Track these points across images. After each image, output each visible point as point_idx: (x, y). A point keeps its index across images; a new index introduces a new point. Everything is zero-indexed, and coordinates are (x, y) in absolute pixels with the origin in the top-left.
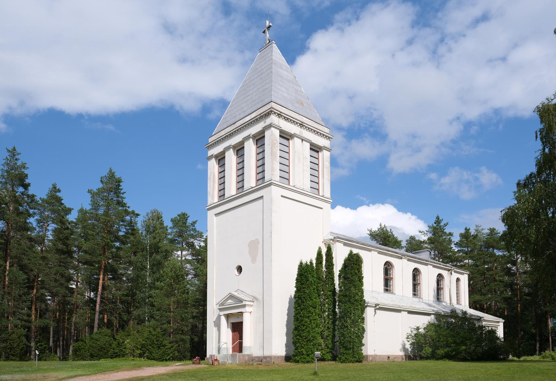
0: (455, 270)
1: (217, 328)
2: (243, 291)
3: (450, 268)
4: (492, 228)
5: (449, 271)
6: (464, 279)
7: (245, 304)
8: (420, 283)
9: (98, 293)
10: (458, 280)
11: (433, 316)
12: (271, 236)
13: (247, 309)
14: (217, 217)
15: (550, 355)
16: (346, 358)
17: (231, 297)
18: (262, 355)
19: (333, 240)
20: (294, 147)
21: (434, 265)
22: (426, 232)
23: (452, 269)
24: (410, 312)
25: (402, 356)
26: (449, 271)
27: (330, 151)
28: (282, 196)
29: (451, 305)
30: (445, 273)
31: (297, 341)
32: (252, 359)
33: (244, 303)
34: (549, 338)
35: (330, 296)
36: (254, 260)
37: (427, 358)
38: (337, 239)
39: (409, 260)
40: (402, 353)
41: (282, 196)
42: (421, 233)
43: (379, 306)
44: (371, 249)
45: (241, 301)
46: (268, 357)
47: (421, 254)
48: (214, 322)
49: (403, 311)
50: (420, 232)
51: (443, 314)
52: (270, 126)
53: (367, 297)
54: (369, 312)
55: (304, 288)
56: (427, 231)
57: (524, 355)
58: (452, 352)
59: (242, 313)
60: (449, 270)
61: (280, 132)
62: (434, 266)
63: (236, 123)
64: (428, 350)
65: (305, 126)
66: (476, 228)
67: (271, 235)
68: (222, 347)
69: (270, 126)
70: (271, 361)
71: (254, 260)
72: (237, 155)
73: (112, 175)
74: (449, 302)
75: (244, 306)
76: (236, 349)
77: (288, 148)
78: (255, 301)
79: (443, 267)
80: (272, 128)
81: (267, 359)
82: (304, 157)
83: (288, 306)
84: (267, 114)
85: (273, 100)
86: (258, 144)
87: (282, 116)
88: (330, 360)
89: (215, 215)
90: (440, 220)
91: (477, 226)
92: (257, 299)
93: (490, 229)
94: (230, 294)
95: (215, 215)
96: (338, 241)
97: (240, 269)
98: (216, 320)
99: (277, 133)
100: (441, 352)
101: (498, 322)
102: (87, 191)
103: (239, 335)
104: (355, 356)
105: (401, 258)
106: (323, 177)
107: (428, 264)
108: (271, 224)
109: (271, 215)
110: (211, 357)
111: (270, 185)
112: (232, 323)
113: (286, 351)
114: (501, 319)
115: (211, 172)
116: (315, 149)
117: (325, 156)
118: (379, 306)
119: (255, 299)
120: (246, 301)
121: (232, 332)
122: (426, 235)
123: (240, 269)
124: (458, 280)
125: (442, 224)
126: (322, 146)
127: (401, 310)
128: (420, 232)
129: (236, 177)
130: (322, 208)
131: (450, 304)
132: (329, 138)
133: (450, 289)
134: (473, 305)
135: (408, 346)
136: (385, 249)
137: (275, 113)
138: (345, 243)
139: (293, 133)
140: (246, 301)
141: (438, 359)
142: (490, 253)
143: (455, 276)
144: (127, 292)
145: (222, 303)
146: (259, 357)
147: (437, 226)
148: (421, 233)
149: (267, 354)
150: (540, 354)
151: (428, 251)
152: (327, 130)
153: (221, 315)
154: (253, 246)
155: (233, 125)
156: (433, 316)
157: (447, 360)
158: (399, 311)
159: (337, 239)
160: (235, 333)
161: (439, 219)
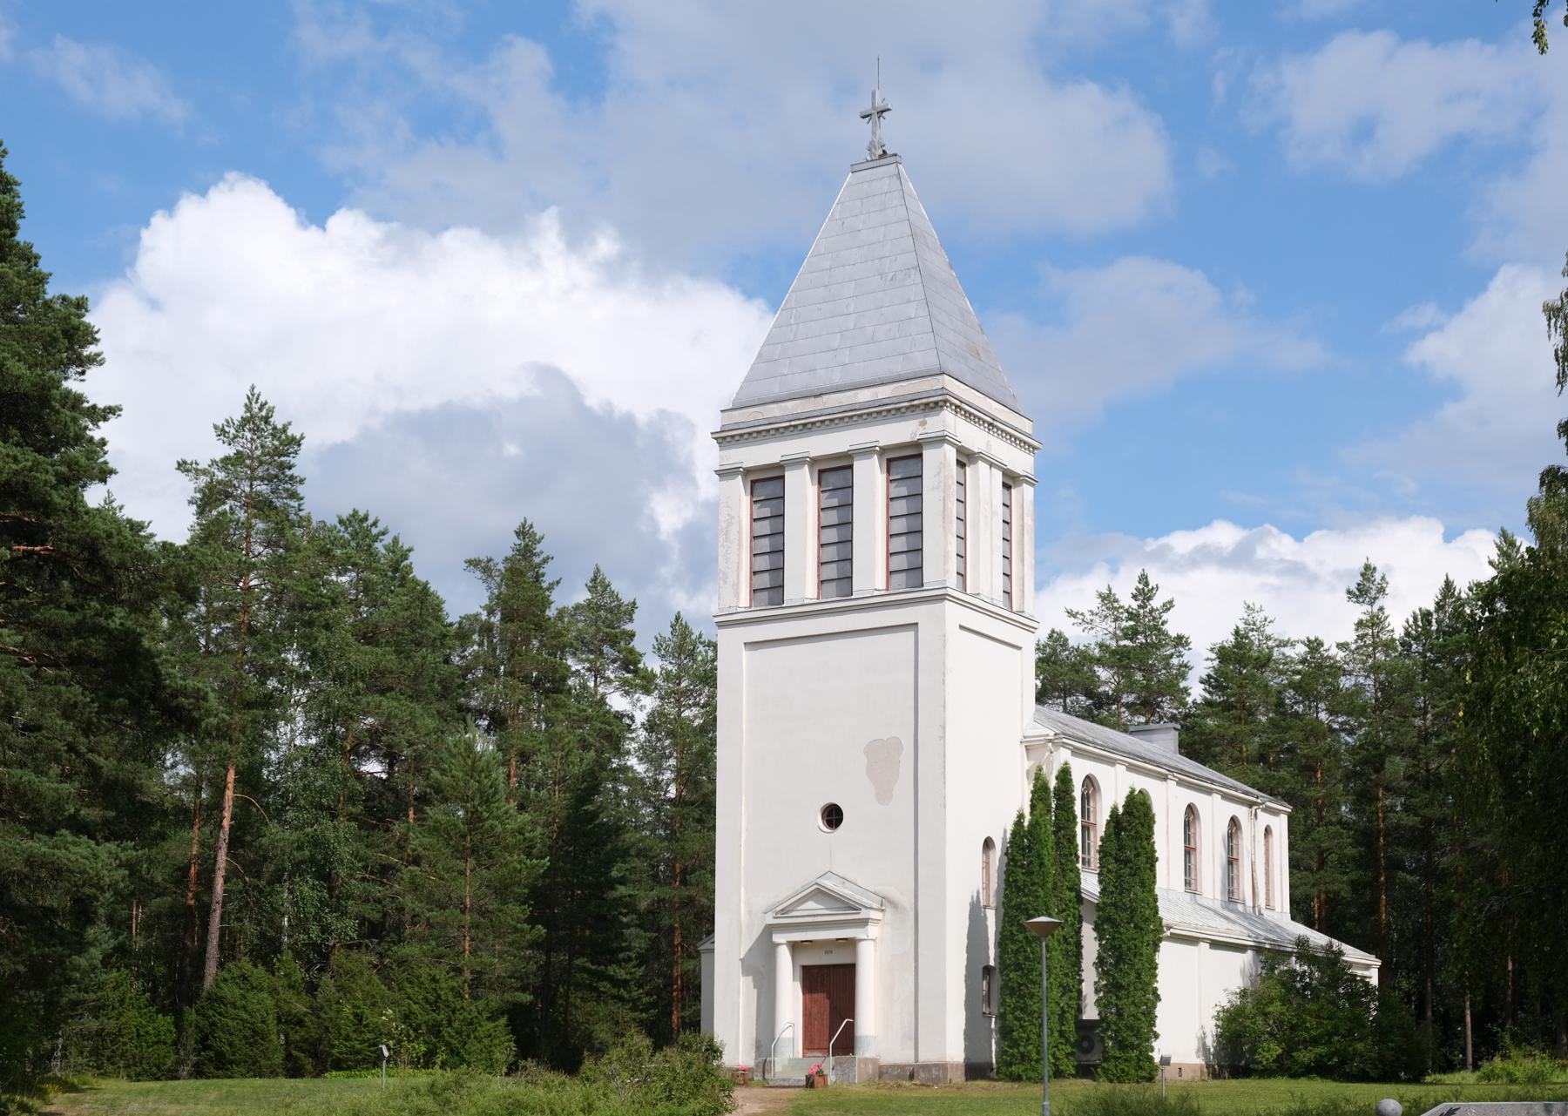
0: (1268, 804)
1: (750, 978)
2: (847, 877)
3: (1254, 799)
4: (1313, 638)
5: (1250, 807)
6: (1280, 825)
7: (868, 919)
8: (1195, 849)
9: (221, 834)
10: (1268, 831)
11: (1250, 953)
12: (943, 737)
13: (872, 931)
14: (750, 650)
15: (1503, 1069)
16: (1123, 1071)
17: (820, 894)
18: (911, 1060)
19: (1053, 743)
20: (977, 487)
21: (1225, 793)
22: (1088, 617)
23: (1259, 801)
24: (1215, 945)
25: (1202, 1066)
26: (1250, 807)
27: (1033, 485)
28: (961, 627)
29: (1254, 912)
30: (1242, 813)
31: (1017, 1023)
32: (883, 1072)
33: (863, 914)
34: (1464, 1017)
35: (1070, 901)
36: (884, 795)
37: (1266, 1073)
38: (1065, 740)
39: (1180, 783)
40: (1200, 1061)
41: (961, 627)
42: (1072, 620)
43: (1172, 930)
44: (1116, 760)
45: (853, 907)
46: (936, 1065)
47: (1154, 736)
48: (741, 960)
49: (1203, 940)
50: (1071, 614)
51: (1267, 946)
52: (940, 440)
53: (1166, 913)
54: (1168, 956)
55: (1034, 884)
56: (1092, 613)
57: (1434, 1072)
58: (1330, 1056)
59: (851, 944)
60: (1250, 805)
61: (958, 451)
62: (1226, 797)
63: (824, 397)
64: (1271, 1051)
65: (996, 426)
66: (1246, 617)
67: (944, 733)
68: (784, 1035)
69: (940, 440)
70: (945, 1078)
71: (884, 795)
72: (819, 483)
73: (256, 418)
74: (1249, 903)
75: (864, 922)
76: (816, 1041)
77: (962, 488)
78: (889, 910)
79: (1240, 798)
80: (946, 446)
81: (930, 1071)
82: (992, 513)
83: (967, 924)
84: (932, 405)
85: (950, 366)
86: (892, 470)
87: (961, 409)
88: (1074, 1076)
89: (745, 644)
90: (1150, 587)
91: (1249, 607)
92: (893, 904)
93: (1309, 641)
94: (816, 886)
95: (745, 644)
96: (1064, 745)
97: (833, 816)
98: (747, 953)
99: (950, 453)
100: (1305, 1056)
101: (1368, 967)
102: (176, 466)
103: (828, 1002)
104: (1141, 1063)
105: (1165, 778)
106: (1022, 560)
107: (1212, 789)
108: (944, 707)
109: (944, 681)
110: (761, 1065)
111: (941, 598)
112: (804, 968)
113: (966, 1050)
114: (1373, 957)
115: (729, 515)
116: (1011, 481)
117: (1026, 493)
118: (1172, 930)
119: (887, 904)
120: (871, 908)
121: (804, 994)
122: (1090, 626)
123: (833, 816)
124: (1268, 831)
125: (1156, 603)
126: (1022, 473)
127: (1199, 938)
128: (1071, 614)
129: (816, 547)
130: (1019, 648)
131: (1254, 907)
132: (1034, 448)
133: (1253, 864)
134: (1300, 910)
135: (1210, 1042)
136: (1129, 753)
137: (952, 404)
138: (1075, 748)
139: (976, 451)
140: (871, 908)
141: (1294, 1076)
142: (1310, 727)
143: (1264, 819)
144: (25, 792)
145: (783, 910)
146: (902, 1067)
147: (1139, 607)
148: (1075, 617)
149: (927, 1056)
150: (1476, 1067)
151: (1175, 729)
152: (1026, 426)
153: (779, 944)
154: (880, 756)
155: (813, 399)
156: (1250, 953)
157: (1318, 1078)
158: (1192, 941)
159: (1065, 740)
160: (815, 995)
161: (1147, 584)
